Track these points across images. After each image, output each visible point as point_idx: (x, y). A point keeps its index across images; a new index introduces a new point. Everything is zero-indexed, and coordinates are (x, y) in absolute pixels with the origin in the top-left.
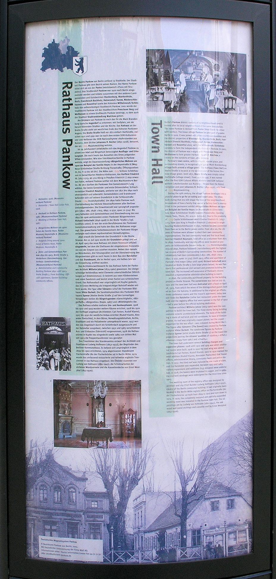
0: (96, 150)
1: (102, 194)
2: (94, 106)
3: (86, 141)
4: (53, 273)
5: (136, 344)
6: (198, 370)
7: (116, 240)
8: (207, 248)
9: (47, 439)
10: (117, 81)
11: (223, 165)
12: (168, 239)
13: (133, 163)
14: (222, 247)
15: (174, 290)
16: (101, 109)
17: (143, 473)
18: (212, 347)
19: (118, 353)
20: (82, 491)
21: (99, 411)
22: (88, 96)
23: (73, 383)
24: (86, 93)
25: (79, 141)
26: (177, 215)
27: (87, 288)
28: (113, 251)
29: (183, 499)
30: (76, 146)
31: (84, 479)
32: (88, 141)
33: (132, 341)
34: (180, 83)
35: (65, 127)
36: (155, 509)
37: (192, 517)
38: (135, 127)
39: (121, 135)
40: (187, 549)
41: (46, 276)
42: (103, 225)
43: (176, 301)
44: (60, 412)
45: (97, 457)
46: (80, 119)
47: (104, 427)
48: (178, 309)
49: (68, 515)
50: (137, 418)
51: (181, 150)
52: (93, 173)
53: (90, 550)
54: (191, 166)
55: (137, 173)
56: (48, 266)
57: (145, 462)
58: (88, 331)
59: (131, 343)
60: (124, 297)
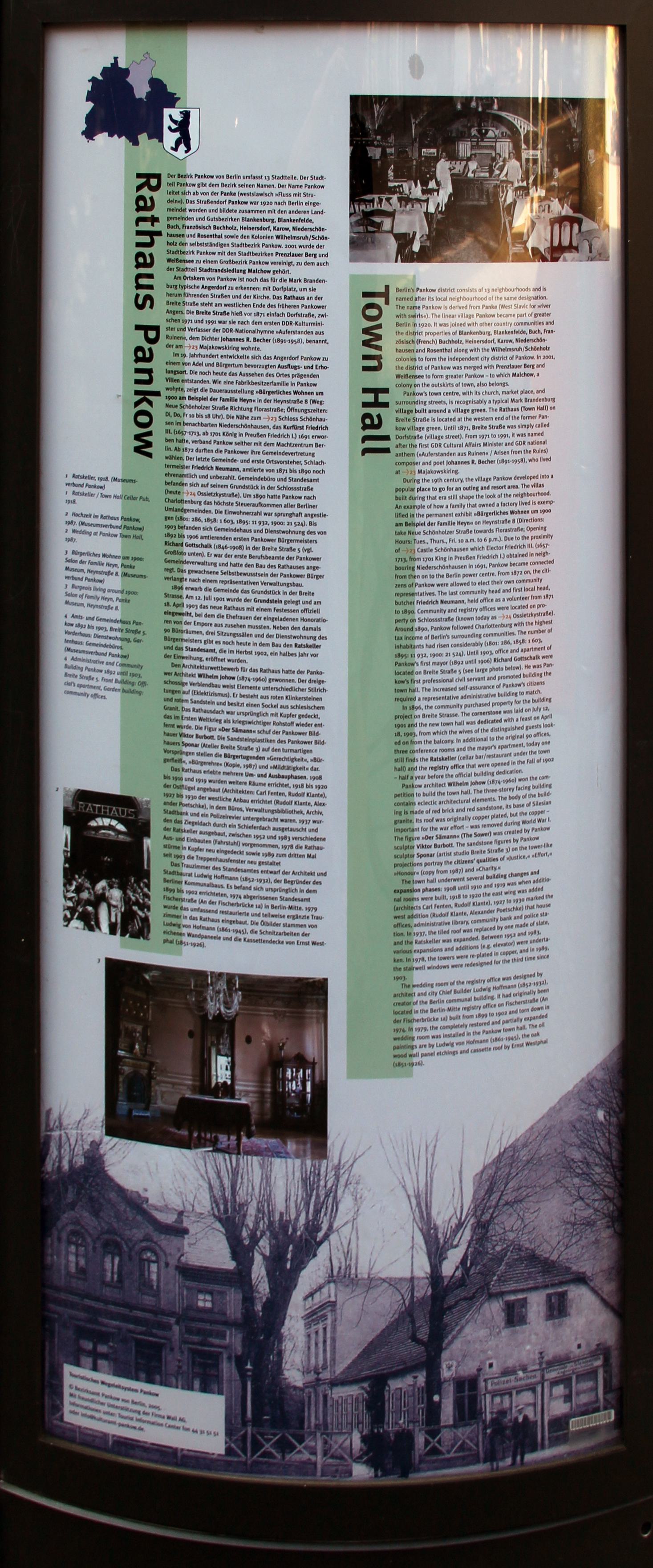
0: (220, 360)
1: (232, 478)
2: (215, 241)
3: (195, 334)
4: (107, 676)
5: (315, 883)
6: (476, 952)
7: (268, 601)
8: (502, 625)
9: (87, 1113)
10: (274, 177)
11: (546, 400)
12: (403, 603)
13: (314, 397)
14: (541, 619)
15: (416, 739)
16: (233, 250)
17: (330, 1228)
18: (512, 888)
19: (269, 903)
20: (173, 1262)
21: (219, 1053)
22: (201, 215)
23: (155, 973)
24: (196, 206)
25: (176, 333)
26: (427, 538)
27: (192, 724)
28: (260, 632)
29: (434, 1297)
30: (168, 346)
31: (179, 1231)
32: (200, 335)
33: (305, 873)
34: (438, 184)
35: (143, 293)
36: (359, 1324)
37: (457, 1345)
38: (318, 303)
39: (284, 323)
40: (444, 1431)
41: (92, 683)
42: (234, 561)
43: (422, 768)
44: (122, 1045)
45: (212, 1174)
46: (181, 274)
47: (233, 1097)
48: (427, 790)
49: (137, 1321)
50: (317, 1079)
51: (437, 364)
52: (211, 421)
53: (190, 1421)
54: (463, 407)
55: (323, 424)
56: (94, 657)
57: (335, 1197)
58: (195, 841)
59: (302, 878)
60: (287, 755)
